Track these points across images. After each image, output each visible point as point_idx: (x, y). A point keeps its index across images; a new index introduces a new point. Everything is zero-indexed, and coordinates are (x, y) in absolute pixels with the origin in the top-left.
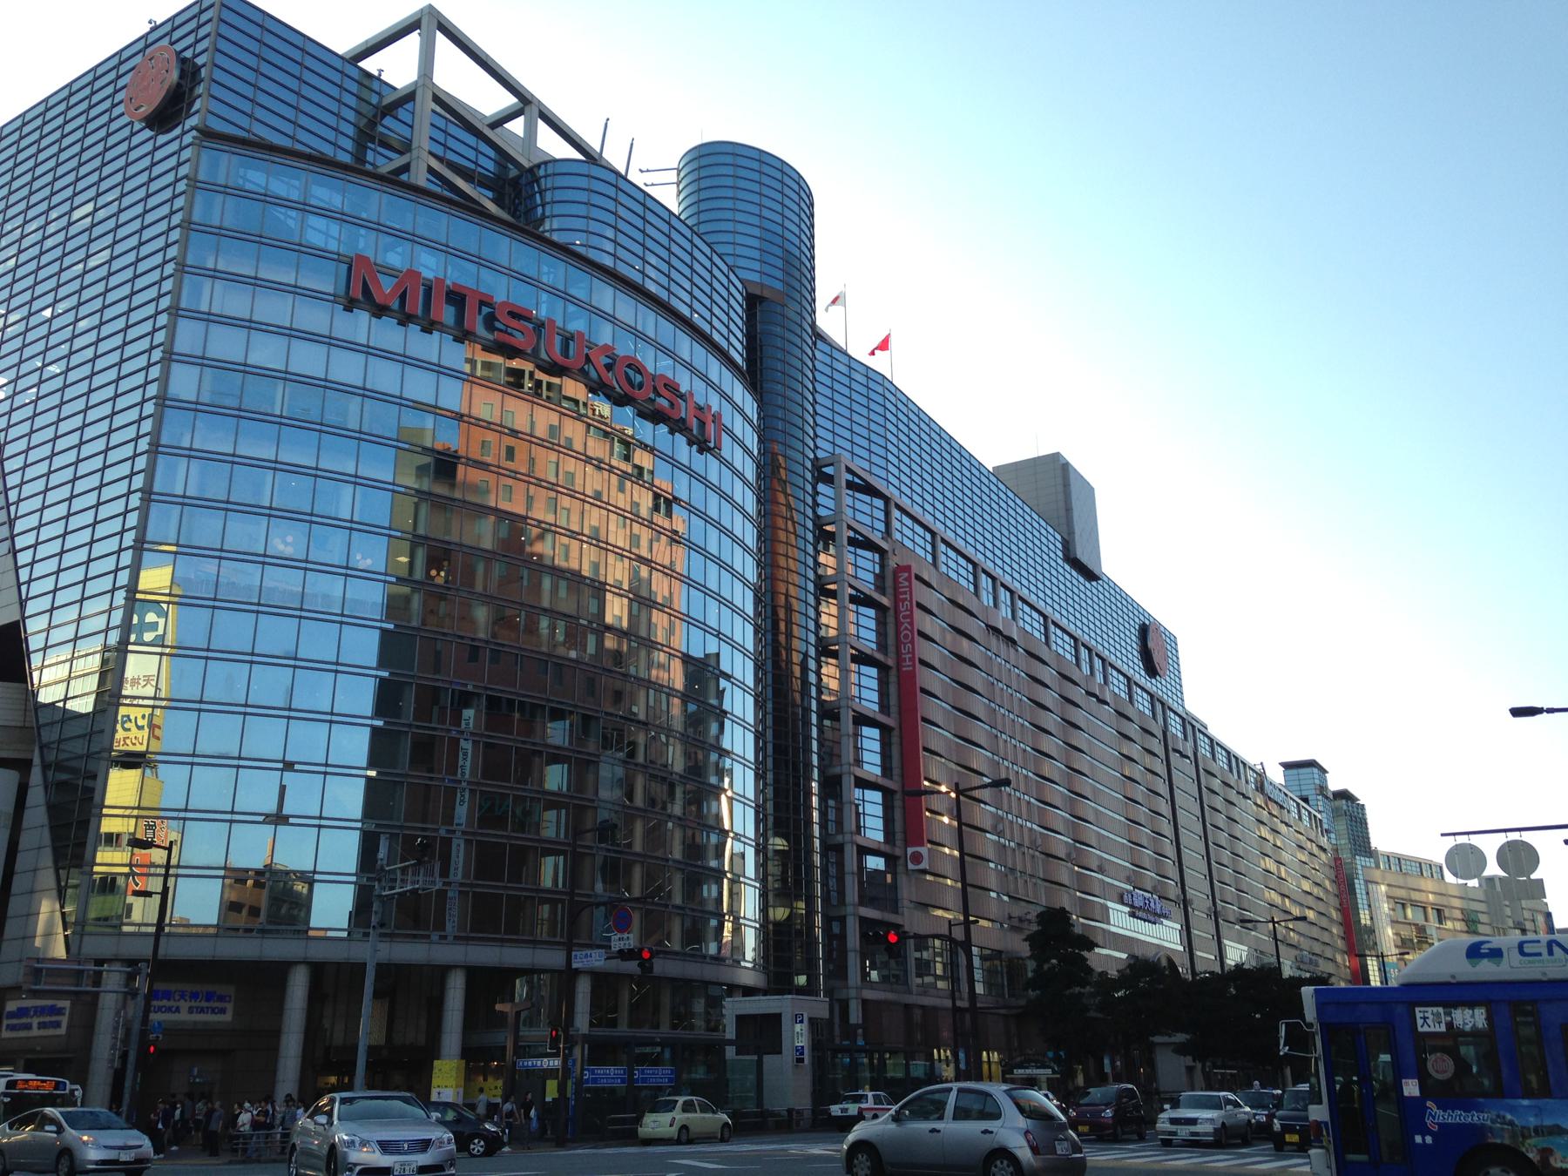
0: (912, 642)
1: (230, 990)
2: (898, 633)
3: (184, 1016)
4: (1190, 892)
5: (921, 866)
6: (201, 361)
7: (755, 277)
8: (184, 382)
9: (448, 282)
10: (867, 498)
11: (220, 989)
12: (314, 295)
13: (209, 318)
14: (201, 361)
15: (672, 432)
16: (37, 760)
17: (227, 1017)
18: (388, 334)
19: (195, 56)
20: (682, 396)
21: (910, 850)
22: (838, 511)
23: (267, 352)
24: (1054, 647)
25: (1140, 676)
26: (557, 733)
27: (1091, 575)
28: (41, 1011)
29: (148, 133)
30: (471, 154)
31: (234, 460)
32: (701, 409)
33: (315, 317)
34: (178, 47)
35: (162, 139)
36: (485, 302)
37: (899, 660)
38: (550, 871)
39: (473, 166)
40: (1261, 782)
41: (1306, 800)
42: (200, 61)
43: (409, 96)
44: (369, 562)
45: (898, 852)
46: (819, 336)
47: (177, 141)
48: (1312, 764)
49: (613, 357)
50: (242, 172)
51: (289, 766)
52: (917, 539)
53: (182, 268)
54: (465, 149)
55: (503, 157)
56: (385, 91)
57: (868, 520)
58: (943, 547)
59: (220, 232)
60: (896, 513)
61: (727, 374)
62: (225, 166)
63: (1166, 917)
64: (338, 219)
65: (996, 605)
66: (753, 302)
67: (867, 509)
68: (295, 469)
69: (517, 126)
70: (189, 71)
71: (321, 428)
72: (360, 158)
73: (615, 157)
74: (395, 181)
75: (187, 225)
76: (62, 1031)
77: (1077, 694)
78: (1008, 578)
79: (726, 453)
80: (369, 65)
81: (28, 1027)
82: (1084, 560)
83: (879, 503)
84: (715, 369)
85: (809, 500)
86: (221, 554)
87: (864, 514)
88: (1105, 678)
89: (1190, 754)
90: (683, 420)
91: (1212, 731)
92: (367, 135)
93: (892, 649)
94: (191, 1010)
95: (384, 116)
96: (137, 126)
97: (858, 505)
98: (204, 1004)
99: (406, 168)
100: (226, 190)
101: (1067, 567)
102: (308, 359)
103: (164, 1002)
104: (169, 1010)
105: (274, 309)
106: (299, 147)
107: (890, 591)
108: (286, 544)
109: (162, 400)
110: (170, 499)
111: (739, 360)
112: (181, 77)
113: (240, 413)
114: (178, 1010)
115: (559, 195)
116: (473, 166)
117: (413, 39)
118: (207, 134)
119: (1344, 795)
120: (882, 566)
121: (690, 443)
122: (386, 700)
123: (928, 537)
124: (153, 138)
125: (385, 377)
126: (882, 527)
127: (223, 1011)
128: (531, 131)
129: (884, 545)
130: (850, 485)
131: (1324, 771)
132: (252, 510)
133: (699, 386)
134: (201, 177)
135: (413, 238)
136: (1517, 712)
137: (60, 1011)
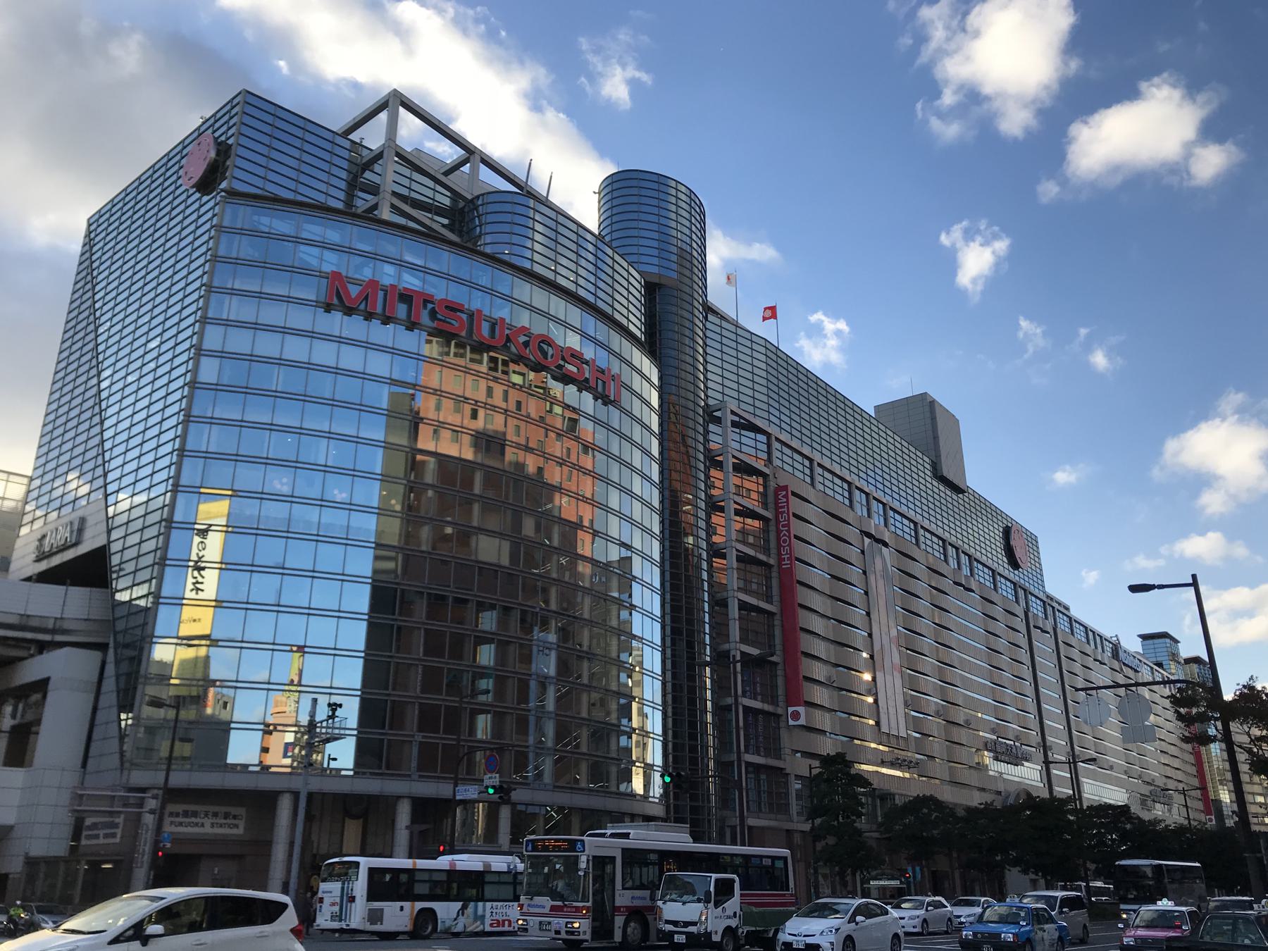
0: (789, 545)
1: (241, 811)
2: (778, 539)
3: (208, 829)
4: (1049, 739)
6: (222, 355)
7: (655, 270)
8: (209, 371)
9: (400, 287)
10: (752, 435)
12: (302, 302)
13: (227, 323)
14: (222, 355)
15: (580, 390)
16: (111, 645)
18: (354, 327)
20: (587, 363)
21: (791, 709)
22: (725, 445)
23: (268, 345)
24: (923, 546)
25: (1003, 566)
26: (488, 621)
27: (958, 489)
29: (198, 195)
30: (430, 193)
31: (241, 424)
32: (603, 372)
33: (301, 318)
34: (217, 135)
35: (205, 198)
36: (427, 300)
37: (780, 560)
38: (483, 726)
40: (1116, 650)
41: (1160, 665)
42: (230, 142)
43: (379, 156)
44: (344, 495)
45: (780, 711)
46: (709, 309)
48: (1164, 635)
49: (529, 335)
50: (256, 218)
51: (301, 649)
53: (209, 288)
54: (424, 189)
55: (455, 195)
56: (365, 152)
57: (753, 452)
59: (236, 262)
61: (626, 344)
62: (243, 215)
63: (1027, 761)
64: (328, 248)
65: (869, 516)
66: (652, 289)
67: (752, 443)
68: (286, 429)
70: (224, 150)
71: (304, 398)
72: (349, 203)
74: (369, 217)
75: (215, 259)
76: (117, 840)
77: (946, 584)
79: (625, 403)
81: (97, 837)
82: (950, 477)
84: (617, 341)
85: (701, 439)
86: (261, 496)
87: (748, 447)
88: (971, 570)
89: (1049, 629)
90: (587, 380)
91: (1074, 613)
92: (354, 184)
94: (212, 825)
95: (363, 171)
96: (191, 191)
97: (744, 440)
99: (375, 207)
100: (241, 232)
101: (935, 483)
102: (296, 349)
103: (193, 820)
104: (197, 824)
105: (272, 314)
107: (771, 505)
108: (282, 484)
109: (193, 385)
110: (197, 454)
111: (638, 333)
112: (218, 154)
113: (247, 391)
114: (203, 825)
115: (490, 218)
118: (232, 193)
120: (765, 487)
121: (596, 399)
122: (385, 598)
124: (200, 199)
125: (352, 358)
126: (765, 456)
127: (236, 826)
128: (474, 171)
129: (766, 471)
130: (734, 424)
131: (1177, 642)
132: (253, 460)
133: (602, 353)
135: (374, 257)
136: (1135, 589)
137: (116, 826)
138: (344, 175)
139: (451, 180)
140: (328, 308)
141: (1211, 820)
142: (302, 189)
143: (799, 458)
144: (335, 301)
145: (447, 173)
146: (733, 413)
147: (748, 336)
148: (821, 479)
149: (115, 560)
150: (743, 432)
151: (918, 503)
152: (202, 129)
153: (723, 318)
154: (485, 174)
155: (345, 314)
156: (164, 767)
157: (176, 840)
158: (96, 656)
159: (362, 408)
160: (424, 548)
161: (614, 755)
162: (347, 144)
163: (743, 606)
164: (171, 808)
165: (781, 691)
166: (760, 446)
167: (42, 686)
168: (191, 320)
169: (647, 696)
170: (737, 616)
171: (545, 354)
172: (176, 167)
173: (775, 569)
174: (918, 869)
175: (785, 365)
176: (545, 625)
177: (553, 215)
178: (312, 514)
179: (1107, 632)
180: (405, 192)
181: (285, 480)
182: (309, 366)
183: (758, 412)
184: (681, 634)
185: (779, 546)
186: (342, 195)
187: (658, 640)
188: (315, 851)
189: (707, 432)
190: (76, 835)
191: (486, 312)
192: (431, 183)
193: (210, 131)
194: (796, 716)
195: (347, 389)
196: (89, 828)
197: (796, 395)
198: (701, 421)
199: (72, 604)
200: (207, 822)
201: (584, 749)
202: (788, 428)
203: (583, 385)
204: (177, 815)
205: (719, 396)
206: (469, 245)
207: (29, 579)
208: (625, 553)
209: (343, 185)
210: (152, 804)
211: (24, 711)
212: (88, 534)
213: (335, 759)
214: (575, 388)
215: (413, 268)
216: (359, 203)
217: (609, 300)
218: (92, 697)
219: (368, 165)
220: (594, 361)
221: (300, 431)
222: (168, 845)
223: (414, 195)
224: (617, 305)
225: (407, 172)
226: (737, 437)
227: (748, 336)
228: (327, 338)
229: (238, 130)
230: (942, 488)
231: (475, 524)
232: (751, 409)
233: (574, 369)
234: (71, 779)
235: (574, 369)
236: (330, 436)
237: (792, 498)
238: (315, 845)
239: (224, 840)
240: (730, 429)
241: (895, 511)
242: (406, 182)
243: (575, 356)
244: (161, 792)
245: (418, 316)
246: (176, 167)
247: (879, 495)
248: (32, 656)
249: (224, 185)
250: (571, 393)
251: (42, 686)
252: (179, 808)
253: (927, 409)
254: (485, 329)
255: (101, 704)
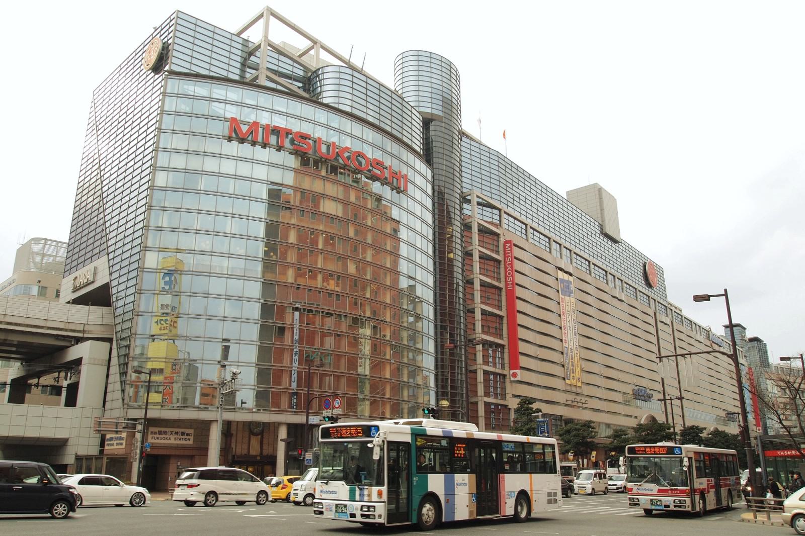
0: (512, 276)
1: (191, 431)
2: (506, 272)
5: (516, 379)
6: (168, 169)
7: (429, 111)
9: (272, 126)
10: (490, 210)
11: (187, 431)
13: (172, 151)
14: (168, 169)
15: (382, 184)
16: (114, 339)
17: (191, 442)
18: (246, 150)
19: (168, 40)
20: (386, 168)
21: (512, 372)
24: (593, 275)
25: (641, 286)
26: (330, 323)
27: (615, 241)
28: (117, 439)
29: (153, 74)
30: (290, 68)
34: (162, 38)
35: (157, 76)
36: (288, 132)
37: (507, 285)
39: (291, 73)
40: (708, 332)
42: (170, 42)
43: (259, 47)
45: (505, 372)
46: (463, 134)
47: (159, 78)
50: (186, 87)
52: (517, 228)
54: (286, 66)
55: (306, 69)
58: (574, 256)
60: (592, 266)
62: (174, 85)
67: (490, 215)
69: (312, 52)
72: (242, 77)
73: (357, 62)
74: (253, 84)
76: (123, 446)
78: (620, 275)
80: (244, 36)
81: (112, 445)
83: (497, 212)
93: (503, 279)
97: (485, 213)
98: (181, 437)
99: (257, 78)
101: (602, 238)
103: (164, 436)
106: (212, 74)
111: (418, 149)
114: (170, 439)
116: (291, 73)
117: (262, 21)
118: (172, 73)
119: (756, 339)
121: (392, 190)
123: (587, 263)
125: (244, 169)
127: (189, 440)
128: (318, 54)
130: (479, 204)
131: (745, 329)
133: (395, 162)
134: (168, 91)
135: (256, 108)
137: (122, 439)
138: (239, 59)
139: (305, 60)
140: (230, 139)
141: (759, 430)
142: (213, 68)
143: (543, 237)
144: (234, 135)
145: (301, 56)
146: (478, 197)
147: (487, 149)
148: (506, 222)
149: (114, 291)
150: (484, 208)
151: (607, 260)
152: (154, 35)
153: (471, 139)
154: (324, 55)
155: (240, 143)
156: (145, 407)
157: (153, 447)
158: (107, 345)
159: (250, 198)
160: (290, 281)
161: (406, 399)
162: (241, 41)
163: (484, 312)
164: (151, 429)
165: (506, 361)
166: (495, 216)
167: (78, 362)
168: (151, 149)
169: (425, 330)
170: (480, 318)
171: (360, 164)
172: (140, 58)
173: (504, 290)
174: (585, 461)
175: (510, 167)
176: (363, 326)
177: (364, 78)
178: (225, 262)
179: (704, 325)
180: (275, 68)
181: (208, 242)
182: (219, 175)
183: (494, 196)
184: (446, 329)
185: (506, 277)
186: (238, 72)
187: (431, 300)
188: (234, 454)
189: (462, 209)
190: (102, 444)
191: (324, 139)
192: (291, 62)
193: (159, 35)
194: (515, 375)
195: (242, 188)
196: (108, 440)
197: (535, 193)
198: (458, 202)
199: (91, 317)
200: (172, 437)
201: (388, 396)
202: (548, 227)
203: (384, 182)
204: (155, 433)
205: (470, 187)
206: (314, 99)
207: (68, 302)
208: (412, 283)
209: (238, 65)
210: (139, 427)
211: (71, 377)
212: (99, 276)
213: (245, 403)
214: (380, 184)
215: (280, 113)
216: (248, 75)
217: (400, 130)
218: (106, 367)
219: (251, 54)
220: (390, 167)
221: (215, 213)
222: (149, 450)
223: (281, 70)
224: (404, 132)
225: (276, 56)
226: (481, 212)
227: (487, 149)
228: (229, 157)
229: (174, 34)
230: (605, 240)
231: (319, 266)
232: (489, 194)
233: (379, 172)
234: (97, 413)
235: (379, 172)
236: (233, 216)
237: (515, 248)
238: (234, 450)
239: (183, 448)
240: (476, 206)
241: (534, 229)
242: (276, 62)
243: (379, 164)
244: (143, 421)
245: (283, 142)
246: (140, 58)
247: (568, 245)
248: (73, 345)
249: (167, 68)
250: (376, 187)
251: (78, 362)
252: (156, 430)
253: (597, 193)
254: (324, 149)
255: (111, 372)
